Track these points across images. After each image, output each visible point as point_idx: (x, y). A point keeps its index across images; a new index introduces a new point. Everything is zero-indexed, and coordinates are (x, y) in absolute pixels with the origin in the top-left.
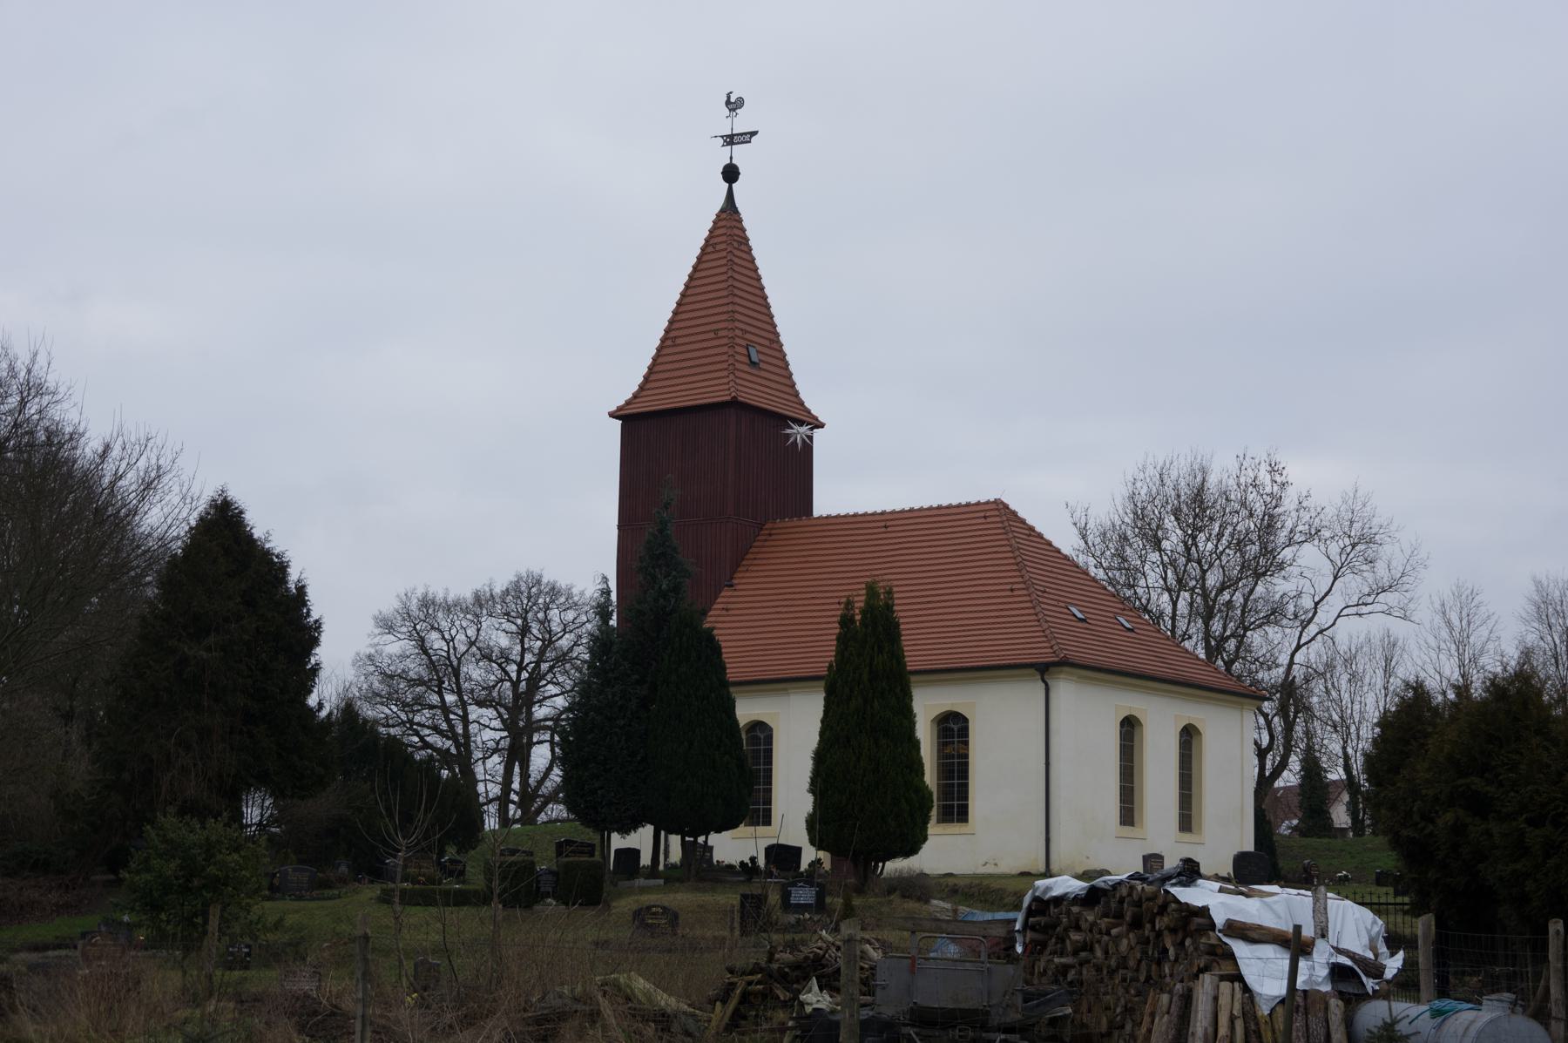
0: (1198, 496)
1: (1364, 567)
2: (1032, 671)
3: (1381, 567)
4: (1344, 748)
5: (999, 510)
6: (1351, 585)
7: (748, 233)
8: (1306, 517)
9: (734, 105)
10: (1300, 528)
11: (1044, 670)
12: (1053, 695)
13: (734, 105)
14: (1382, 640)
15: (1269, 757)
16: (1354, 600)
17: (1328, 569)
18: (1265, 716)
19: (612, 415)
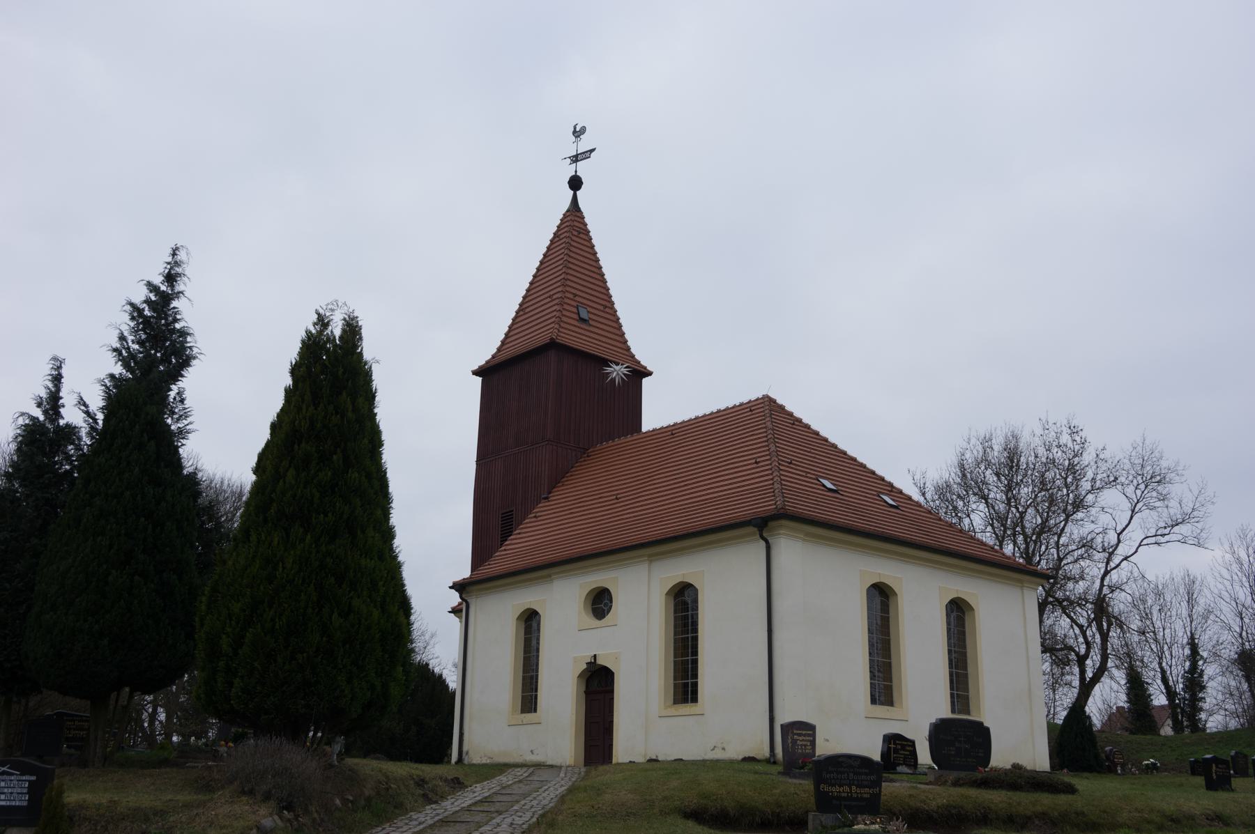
0: (1012, 455)
1: (1158, 504)
2: (751, 529)
3: (1173, 503)
4: (1160, 664)
5: (767, 409)
6: (1148, 520)
7: (589, 227)
8: (1104, 467)
9: (578, 133)
10: (1099, 477)
11: (762, 526)
12: (774, 553)
13: (578, 133)
14: (1183, 579)
15: (1089, 662)
16: (1153, 532)
17: (1127, 506)
18: (1081, 627)
19: (476, 373)
